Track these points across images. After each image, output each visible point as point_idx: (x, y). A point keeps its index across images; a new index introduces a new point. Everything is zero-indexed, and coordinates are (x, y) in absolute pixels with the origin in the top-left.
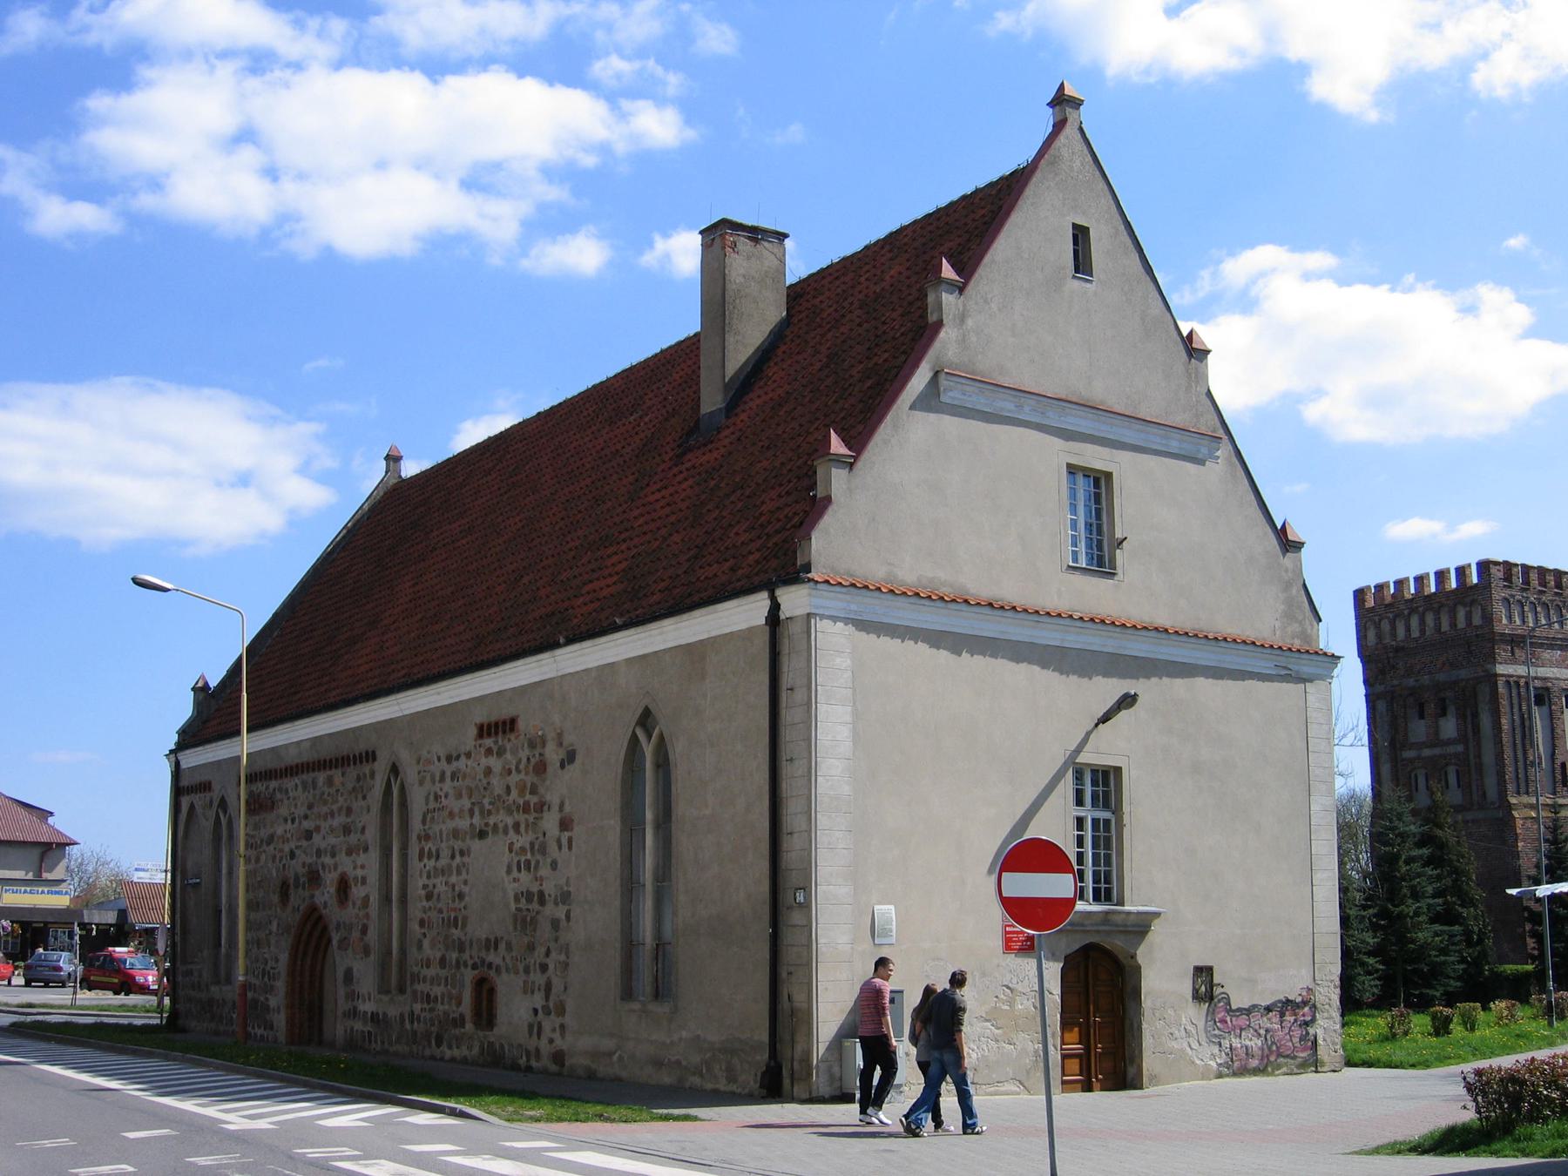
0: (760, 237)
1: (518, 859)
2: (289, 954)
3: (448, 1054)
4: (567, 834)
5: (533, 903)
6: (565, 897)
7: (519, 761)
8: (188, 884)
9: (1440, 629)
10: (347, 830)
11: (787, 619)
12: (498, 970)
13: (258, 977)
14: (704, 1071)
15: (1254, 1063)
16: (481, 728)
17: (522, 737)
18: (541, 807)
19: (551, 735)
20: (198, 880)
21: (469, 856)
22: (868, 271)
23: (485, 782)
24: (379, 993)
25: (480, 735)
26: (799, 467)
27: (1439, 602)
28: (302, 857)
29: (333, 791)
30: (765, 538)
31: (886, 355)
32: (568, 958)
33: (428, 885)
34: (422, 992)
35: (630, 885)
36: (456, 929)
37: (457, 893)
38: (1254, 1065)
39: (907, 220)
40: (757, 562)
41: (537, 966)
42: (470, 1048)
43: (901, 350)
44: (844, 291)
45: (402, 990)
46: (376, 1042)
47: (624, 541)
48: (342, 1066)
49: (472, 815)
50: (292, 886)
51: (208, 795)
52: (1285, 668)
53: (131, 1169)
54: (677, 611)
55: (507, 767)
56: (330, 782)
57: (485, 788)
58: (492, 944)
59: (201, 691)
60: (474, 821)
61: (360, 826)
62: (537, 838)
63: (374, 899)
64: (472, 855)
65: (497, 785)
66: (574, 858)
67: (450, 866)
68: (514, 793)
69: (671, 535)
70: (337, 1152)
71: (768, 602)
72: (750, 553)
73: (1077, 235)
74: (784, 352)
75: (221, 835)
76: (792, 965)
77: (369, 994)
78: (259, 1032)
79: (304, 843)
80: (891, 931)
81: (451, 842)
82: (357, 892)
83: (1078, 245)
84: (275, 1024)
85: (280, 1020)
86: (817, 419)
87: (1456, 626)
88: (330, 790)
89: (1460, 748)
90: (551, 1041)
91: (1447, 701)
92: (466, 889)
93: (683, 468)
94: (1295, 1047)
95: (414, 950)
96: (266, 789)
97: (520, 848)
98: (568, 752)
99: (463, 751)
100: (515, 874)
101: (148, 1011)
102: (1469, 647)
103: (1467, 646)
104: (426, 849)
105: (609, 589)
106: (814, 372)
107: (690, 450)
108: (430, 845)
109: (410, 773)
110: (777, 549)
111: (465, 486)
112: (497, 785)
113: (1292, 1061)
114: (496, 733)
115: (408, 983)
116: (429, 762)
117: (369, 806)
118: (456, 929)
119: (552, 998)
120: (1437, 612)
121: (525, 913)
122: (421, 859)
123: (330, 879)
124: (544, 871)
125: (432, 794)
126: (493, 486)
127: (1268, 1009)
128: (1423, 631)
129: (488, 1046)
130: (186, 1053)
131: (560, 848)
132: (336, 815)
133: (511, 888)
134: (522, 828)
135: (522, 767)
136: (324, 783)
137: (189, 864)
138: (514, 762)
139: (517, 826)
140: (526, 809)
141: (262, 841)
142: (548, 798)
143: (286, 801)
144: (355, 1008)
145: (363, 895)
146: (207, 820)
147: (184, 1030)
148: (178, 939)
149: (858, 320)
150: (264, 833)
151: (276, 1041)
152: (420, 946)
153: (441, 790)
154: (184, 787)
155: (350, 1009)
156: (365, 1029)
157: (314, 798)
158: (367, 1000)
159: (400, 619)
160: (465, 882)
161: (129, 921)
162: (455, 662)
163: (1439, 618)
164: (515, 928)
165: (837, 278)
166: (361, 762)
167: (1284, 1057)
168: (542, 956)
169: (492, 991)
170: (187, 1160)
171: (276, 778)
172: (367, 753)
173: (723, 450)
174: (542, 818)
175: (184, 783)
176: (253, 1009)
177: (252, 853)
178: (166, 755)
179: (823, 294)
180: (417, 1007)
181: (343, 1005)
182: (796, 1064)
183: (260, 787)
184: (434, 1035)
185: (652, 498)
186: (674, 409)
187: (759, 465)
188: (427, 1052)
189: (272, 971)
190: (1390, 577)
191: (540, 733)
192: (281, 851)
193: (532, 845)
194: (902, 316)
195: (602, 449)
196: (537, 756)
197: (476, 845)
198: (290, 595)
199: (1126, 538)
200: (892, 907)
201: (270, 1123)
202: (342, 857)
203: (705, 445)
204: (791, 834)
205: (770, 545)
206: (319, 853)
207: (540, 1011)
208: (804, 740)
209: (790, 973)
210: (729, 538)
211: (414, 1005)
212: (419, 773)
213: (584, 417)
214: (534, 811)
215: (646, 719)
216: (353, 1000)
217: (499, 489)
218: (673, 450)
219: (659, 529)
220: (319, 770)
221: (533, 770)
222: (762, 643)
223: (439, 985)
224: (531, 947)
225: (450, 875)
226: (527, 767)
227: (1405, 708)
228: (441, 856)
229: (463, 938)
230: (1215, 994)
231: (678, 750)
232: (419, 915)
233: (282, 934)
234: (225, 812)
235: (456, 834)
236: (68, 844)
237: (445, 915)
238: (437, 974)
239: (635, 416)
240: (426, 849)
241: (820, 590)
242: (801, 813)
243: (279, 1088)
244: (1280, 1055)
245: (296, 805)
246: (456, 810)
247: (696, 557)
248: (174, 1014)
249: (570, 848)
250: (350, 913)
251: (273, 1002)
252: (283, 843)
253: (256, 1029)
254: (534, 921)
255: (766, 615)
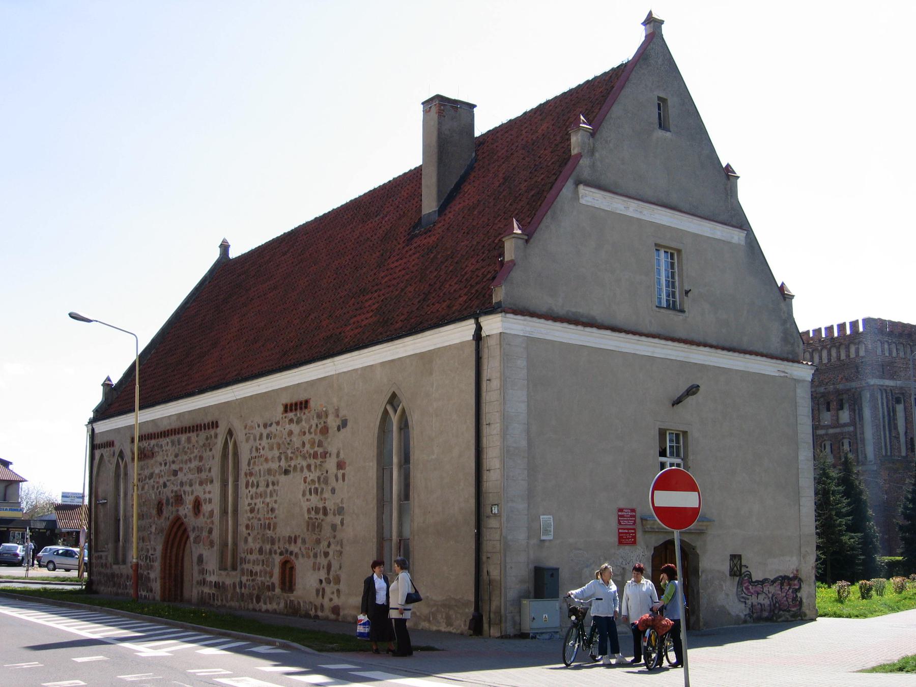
0: (459, 106)
1: (309, 487)
2: (163, 546)
3: (264, 607)
4: (341, 471)
5: (320, 514)
6: (340, 511)
7: (311, 427)
8: (99, 504)
9: (840, 359)
10: (199, 470)
11: (487, 336)
12: (296, 556)
13: (142, 560)
14: (431, 619)
15: (765, 614)
16: (286, 406)
17: (313, 412)
18: (325, 455)
19: (331, 411)
20: (105, 501)
21: (278, 485)
22: (526, 127)
23: (288, 440)
24: (220, 570)
25: (286, 411)
26: (489, 245)
27: (840, 342)
28: (171, 487)
29: (190, 446)
30: (470, 286)
31: (543, 176)
32: (342, 548)
33: (251, 504)
34: (248, 570)
35: (382, 502)
36: (270, 530)
37: (270, 508)
38: (765, 616)
39: (550, 97)
40: (465, 302)
41: (322, 553)
42: (278, 604)
43: (552, 173)
44: (511, 140)
45: (234, 568)
46: (218, 600)
47: (376, 291)
48: (204, 615)
49: (280, 459)
50: (164, 504)
51: (112, 449)
52: (784, 372)
53: (83, 683)
54: (414, 332)
55: (303, 430)
56: (189, 440)
57: (288, 444)
58: (293, 540)
59: (107, 385)
60: (281, 464)
61: (208, 467)
62: (322, 474)
63: (217, 512)
64: (280, 484)
65: (296, 441)
66: (346, 487)
67: (265, 492)
68: (307, 446)
69: (406, 287)
70: (215, 672)
71: (474, 326)
72: (460, 296)
73: (660, 104)
74: (474, 177)
75: (120, 474)
76: (490, 553)
77: (214, 571)
78: (144, 593)
79: (173, 478)
80: (550, 532)
81: (266, 477)
82: (206, 508)
83: (660, 110)
84: (154, 589)
85: (157, 586)
86: (499, 215)
87: (849, 356)
88: (189, 446)
89: (851, 429)
90: (331, 600)
91: (844, 401)
92: (276, 506)
93: (412, 247)
94: (789, 605)
95: (242, 543)
96: (148, 445)
97: (311, 480)
98: (342, 421)
99: (274, 421)
100: (308, 496)
101: (72, 581)
102: (857, 369)
103: (856, 369)
104: (251, 481)
105: (367, 321)
106: (494, 188)
107: (416, 236)
108: (253, 478)
109: (240, 435)
110: (478, 294)
111: (270, 262)
112: (296, 441)
113: (788, 613)
114: (296, 410)
115: (239, 563)
116: (252, 428)
117: (213, 456)
118: (270, 530)
119: (331, 573)
120: (838, 348)
121: (314, 520)
122: (247, 488)
123: (189, 500)
124: (327, 495)
125: (254, 447)
126: (288, 261)
127: (774, 582)
128: (829, 360)
129: (290, 603)
130: (103, 607)
131: (337, 480)
132: (193, 460)
133: (305, 505)
134: (313, 468)
135: (312, 430)
136: (185, 442)
137: (100, 491)
138: (308, 427)
139: (309, 467)
140: (315, 456)
141: (146, 477)
142: (329, 449)
143: (161, 453)
144: (204, 579)
145: (210, 509)
146: (111, 464)
147: (96, 592)
148: (93, 537)
149: (522, 156)
150: (147, 472)
151: (154, 599)
152: (246, 540)
153: (260, 444)
154: (97, 445)
155: (201, 580)
156: (210, 592)
157: (179, 451)
158: (212, 574)
159: (232, 341)
160: (276, 502)
161: (58, 527)
162: (269, 367)
163: (840, 352)
164: (308, 530)
165: (506, 132)
166: (209, 428)
167: (783, 611)
168: (325, 548)
169: (292, 568)
170: (118, 677)
171: (155, 438)
172: (213, 423)
173: (438, 236)
174: (326, 461)
175: (98, 441)
176: (140, 579)
177: (140, 484)
178: (86, 425)
179: (498, 142)
180: (244, 579)
181: (197, 577)
182: (492, 616)
183: (145, 444)
184: (255, 596)
185: (393, 266)
186: (404, 213)
187: (463, 244)
188: (251, 606)
189: (151, 557)
190: (823, 325)
191: (324, 409)
192: (158, 482)
193: (319, 478)
194: (552, 152)
195: (358, 238)
196: (322, 423)
197: (283, 479)
198: (161, 329)
199: (690, 290)
200: (551, 517)
201: (167, 652)
202: (197, 487)
203: (426, 233)
204: (489, 470)
205: (473, 291)
206: (182, 484)
207: (324, 581)
208: (497, 412)
209: (488, 558)
210: (445, 288)
211: (242, 577)
212: (246, 434)
213: (346, 219)
214: (321, 457)
215: (393, 400)
216: (203, 574)
217: (292, 263)
218: (405, 236)
219: (398, 283)
220: (182, 433)
221: (320, 431)
222: (471, 351)
223: (258, 565)
224: (318, 542)
225: (266, 497)
226: (315, 431)
227: (818, 405)
228: (260, 485)
229: (274, 536)
230: (742, 572)
231: (414, 419)
232: (246, 522)
233: (158, 533)
234: (123, 460)
235: (269, 472)
236: (21, 481)
237: (262, 522)
238: (257, 559)
239: (379, 217)
240: (251, 481)
241: (508, 318)
242: (495, 457)
243: (127, 621)
244: (780, 609)
245: (167, 455)
246: (270, 457)
247: (424, 300)
248: (90, 583)
249: (344, 480)
250: (201, 521)
251: (152, 576)
252: (159, 478)
253: (142, 591)
254: (320, 526)
255: (473, 334)
